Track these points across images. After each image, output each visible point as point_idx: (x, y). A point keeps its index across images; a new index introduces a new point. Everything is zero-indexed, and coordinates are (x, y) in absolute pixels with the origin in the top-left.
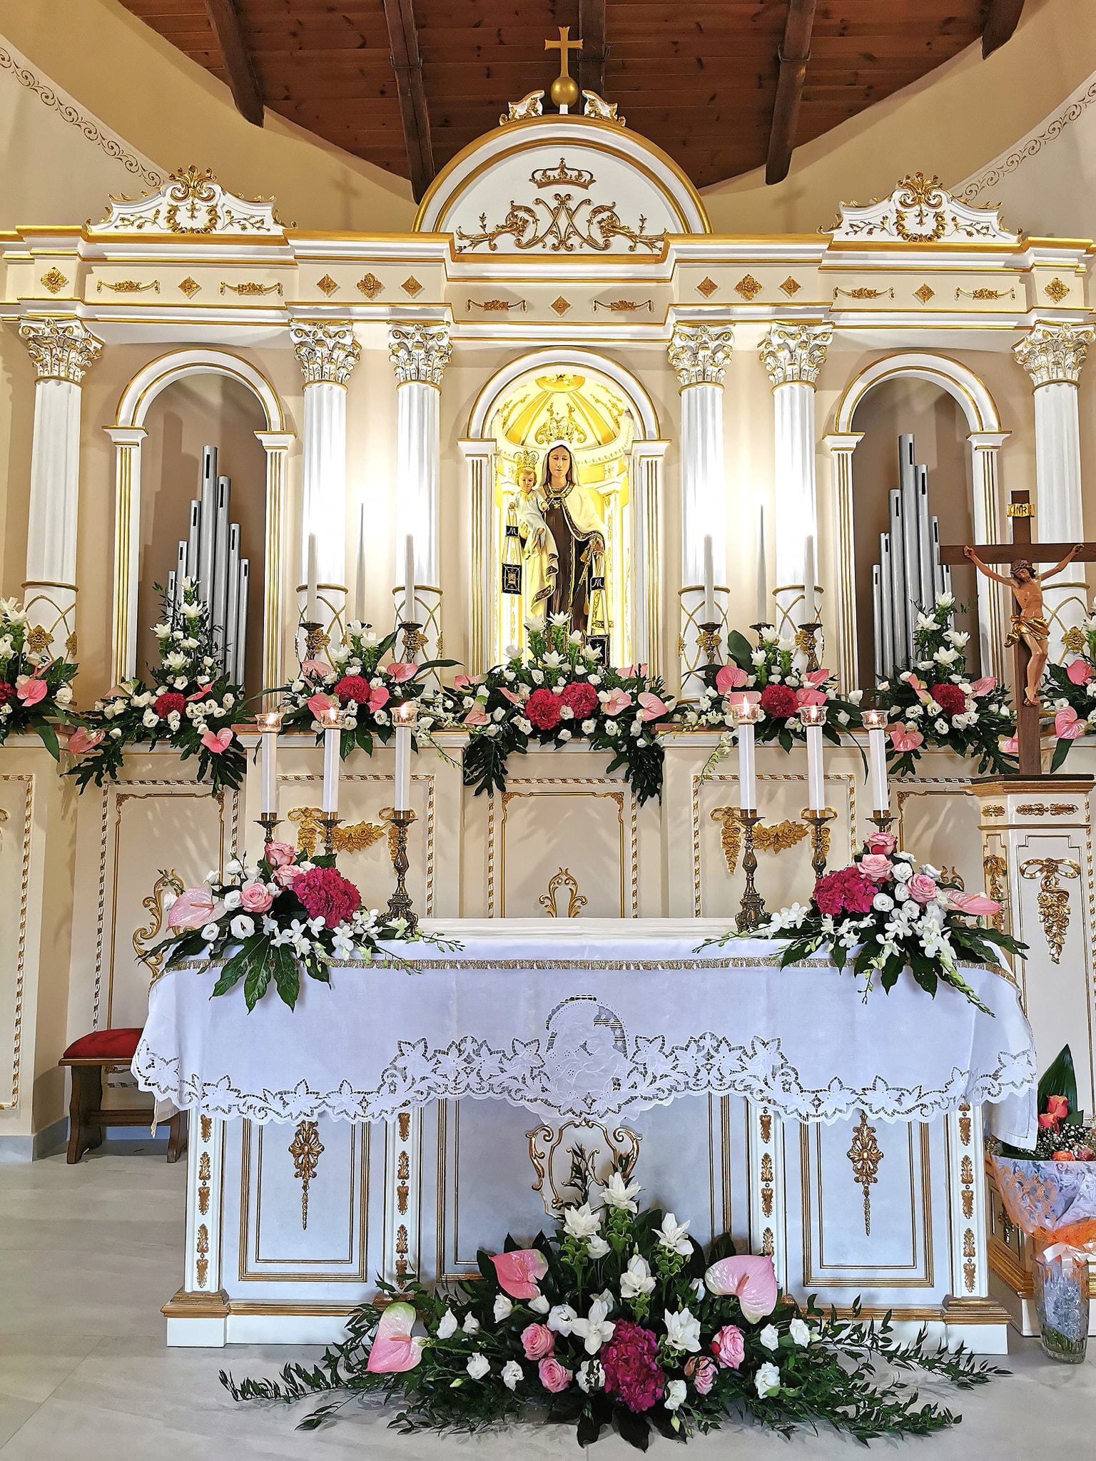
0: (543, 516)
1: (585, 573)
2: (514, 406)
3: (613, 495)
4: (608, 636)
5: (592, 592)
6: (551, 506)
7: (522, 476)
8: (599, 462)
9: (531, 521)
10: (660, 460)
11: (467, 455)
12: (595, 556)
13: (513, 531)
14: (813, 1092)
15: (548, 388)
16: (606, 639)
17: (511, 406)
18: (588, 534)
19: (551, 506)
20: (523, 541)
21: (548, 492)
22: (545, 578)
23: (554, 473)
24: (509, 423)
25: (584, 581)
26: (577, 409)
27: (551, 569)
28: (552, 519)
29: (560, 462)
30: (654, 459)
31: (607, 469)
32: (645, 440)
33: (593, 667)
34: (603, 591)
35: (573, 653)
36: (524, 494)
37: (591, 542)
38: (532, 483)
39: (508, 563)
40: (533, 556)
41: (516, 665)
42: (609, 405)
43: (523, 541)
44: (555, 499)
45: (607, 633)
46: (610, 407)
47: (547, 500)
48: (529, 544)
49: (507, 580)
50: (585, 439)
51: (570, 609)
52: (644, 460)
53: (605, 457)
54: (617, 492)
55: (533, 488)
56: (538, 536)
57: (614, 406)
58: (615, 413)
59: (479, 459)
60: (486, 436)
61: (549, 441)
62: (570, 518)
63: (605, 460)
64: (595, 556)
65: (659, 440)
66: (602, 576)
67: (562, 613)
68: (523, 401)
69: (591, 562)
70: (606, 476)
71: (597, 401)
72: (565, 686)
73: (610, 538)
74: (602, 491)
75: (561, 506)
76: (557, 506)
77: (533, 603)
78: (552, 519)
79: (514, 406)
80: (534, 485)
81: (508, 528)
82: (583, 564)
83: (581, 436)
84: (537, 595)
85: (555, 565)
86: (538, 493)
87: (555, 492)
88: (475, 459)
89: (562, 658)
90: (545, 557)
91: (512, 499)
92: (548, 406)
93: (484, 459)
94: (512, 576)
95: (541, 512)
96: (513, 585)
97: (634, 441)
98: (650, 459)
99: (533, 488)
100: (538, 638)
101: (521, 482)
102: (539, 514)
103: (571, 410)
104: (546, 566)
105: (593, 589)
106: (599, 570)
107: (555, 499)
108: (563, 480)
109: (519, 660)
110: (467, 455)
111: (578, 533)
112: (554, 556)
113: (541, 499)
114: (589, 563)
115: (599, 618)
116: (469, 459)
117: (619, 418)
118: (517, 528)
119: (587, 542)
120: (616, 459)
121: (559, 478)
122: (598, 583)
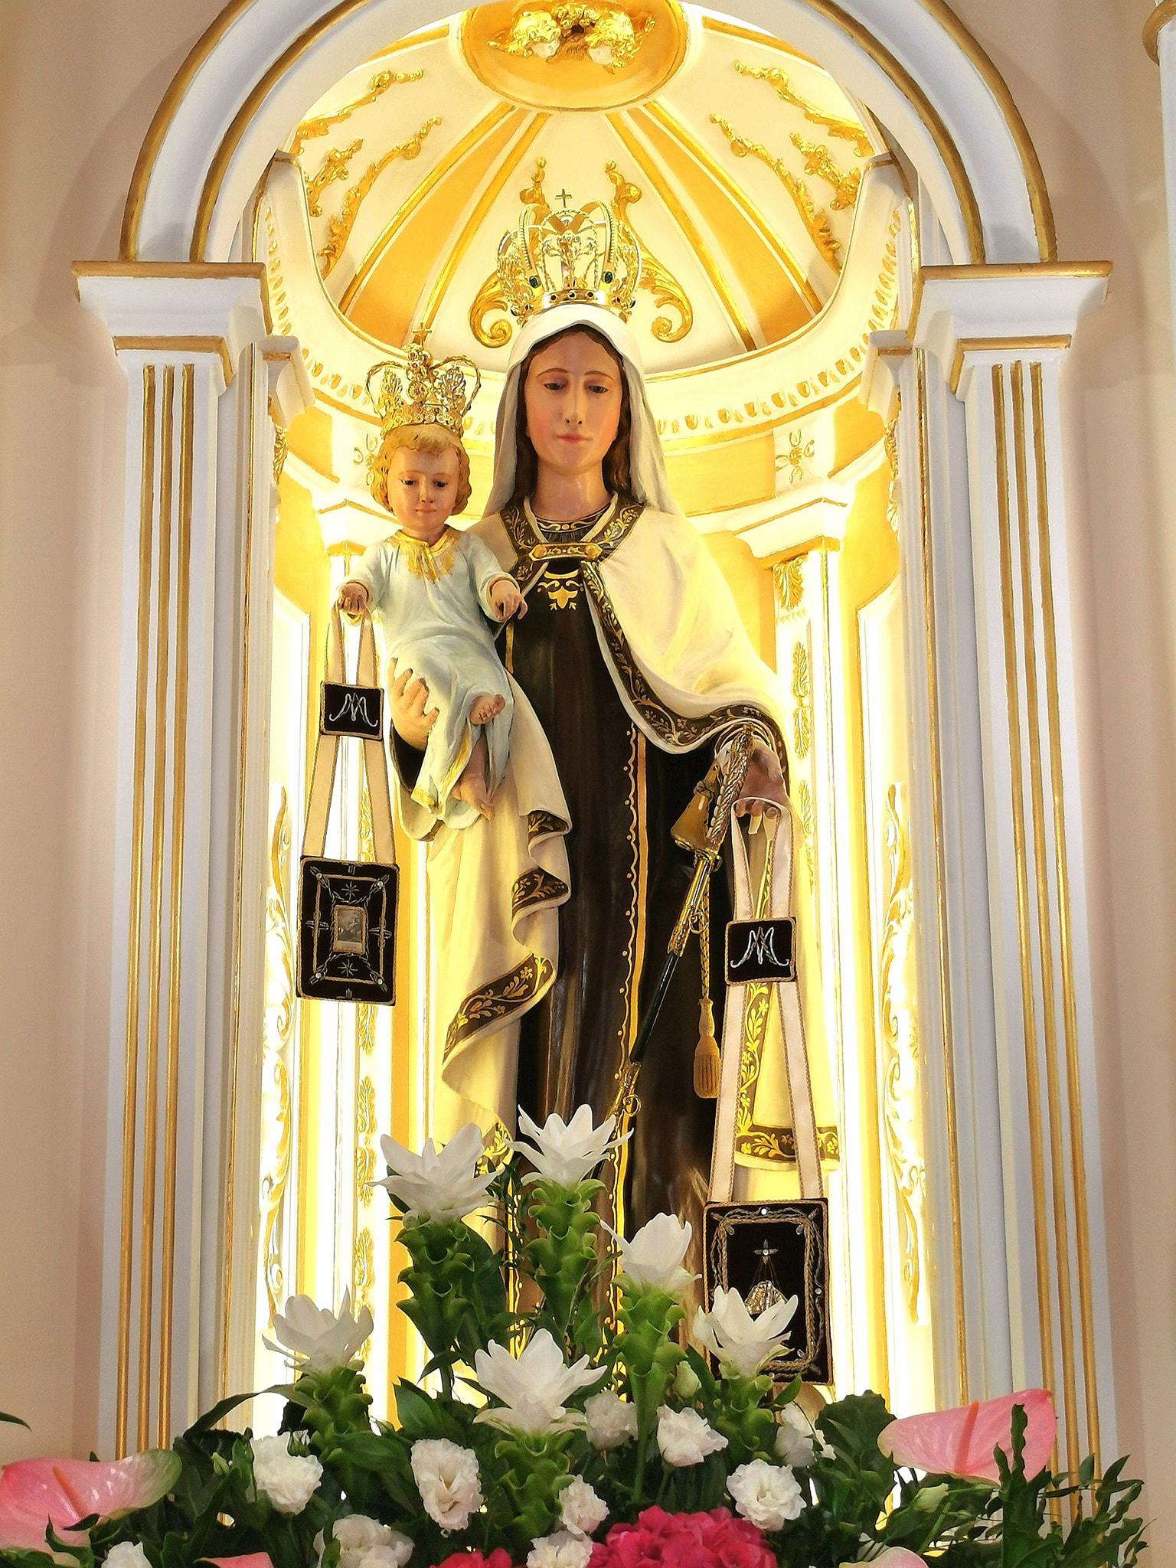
0: (500, 646)
1: (697, 898)
2: (374, 172)
3: (814, 556)
4: (816, 1210)
5: (736, 994)
6: (537, 599)
7: (401, 464)
8: (749, 422)
9: (445, 662)
10: (1055, 362)
11: (123, 343)
12: (744, 822)
13: (355, 710)
14: (767, 1013)
15: (522, 90)
16: (805, 1227)
17: (357, 169)
18: (705, 722)
19: (537, 599)
20: (410, 758)
21: (520, 535)
22: (511, 923)
23: (549, 449)
24: (358, 246)
25: (694, 940)
26: (649, 189)
27: (534, 885)
28: (543, 655)
29: (577, 403)
30: (1028, 356)
31: (783, 446)
32: (980, 262)
33: (755, 1413)
34: (787, 988)
35: (642, 1340)
36: (409, 546)
37: (722, 757)
38: (448, 495)
39: (332, 854)
40: (456, 822)
41: (329, 1403)
42: (795, 164)
43: (410, 758)
44: (557, 566)
45: (812, 1194)
46: (799, 172)
47: (522, 569)
48: (435, 772)
49: (326, 938)
50: (687, 327)
51: (625, 1078)
52: (980, 362)
53: (777, 400)
54: (832, 544)
55: (453, 521)
56: (473, 733)
57: (816, 161)
58: (820, 194)
59: (178, 359)
60: (219, 250)
61: (524, 313)
62: (622, 651)
63: (777, 413)
64: (744, 822)
65: (1053, 260)
66: (779, 914)
67: (585, 1111)
68: (408, 152)
69: (726, 850)
70: (783, 478)
71: (739, 148)
72: (599, 1534)
73: (803, 747)
74: (766, 542)
75: (581, 599)
76: (561, 598)
77: (457, 1034)
78: (543, 655)
79: (374, 172)
80: (459, 505)
81: (334, 695)
82: (687, 858)
83: (671, 313)
84: (471, 1002)
85: (555, 862)
86: (478, 544)
87: (555, 538)
88: (161, 359)
89: (583, 1374)
90: (509, 831)
91: (360, 569)
92: (521, 180)
93: (206, 363)
94: (349, 917)
95: (492, 625)
96: (356, 960)
97: (927, 272)
98: (1006, 358)
99: (453, 521)
100: (455, 1257)
101: (398, 492)
102: (481, 635)
103: (624, 197)
104: (511, 870)
105: (739, 976)
106: (763, 891)
107: (557, 566)
108: (590, 486)
109: (351, 1378)
110: (123, 343)
111: (661, 715)
112: (544, 822)
113: (491, 569)
114: (713, 854)
115: (767, 1114)
116: (131, 364)
117: (839, 221)
118: (374, 697)
119: (703, 758)
120: (823, 404)
121: (568, 473)
122: (759, 949)
